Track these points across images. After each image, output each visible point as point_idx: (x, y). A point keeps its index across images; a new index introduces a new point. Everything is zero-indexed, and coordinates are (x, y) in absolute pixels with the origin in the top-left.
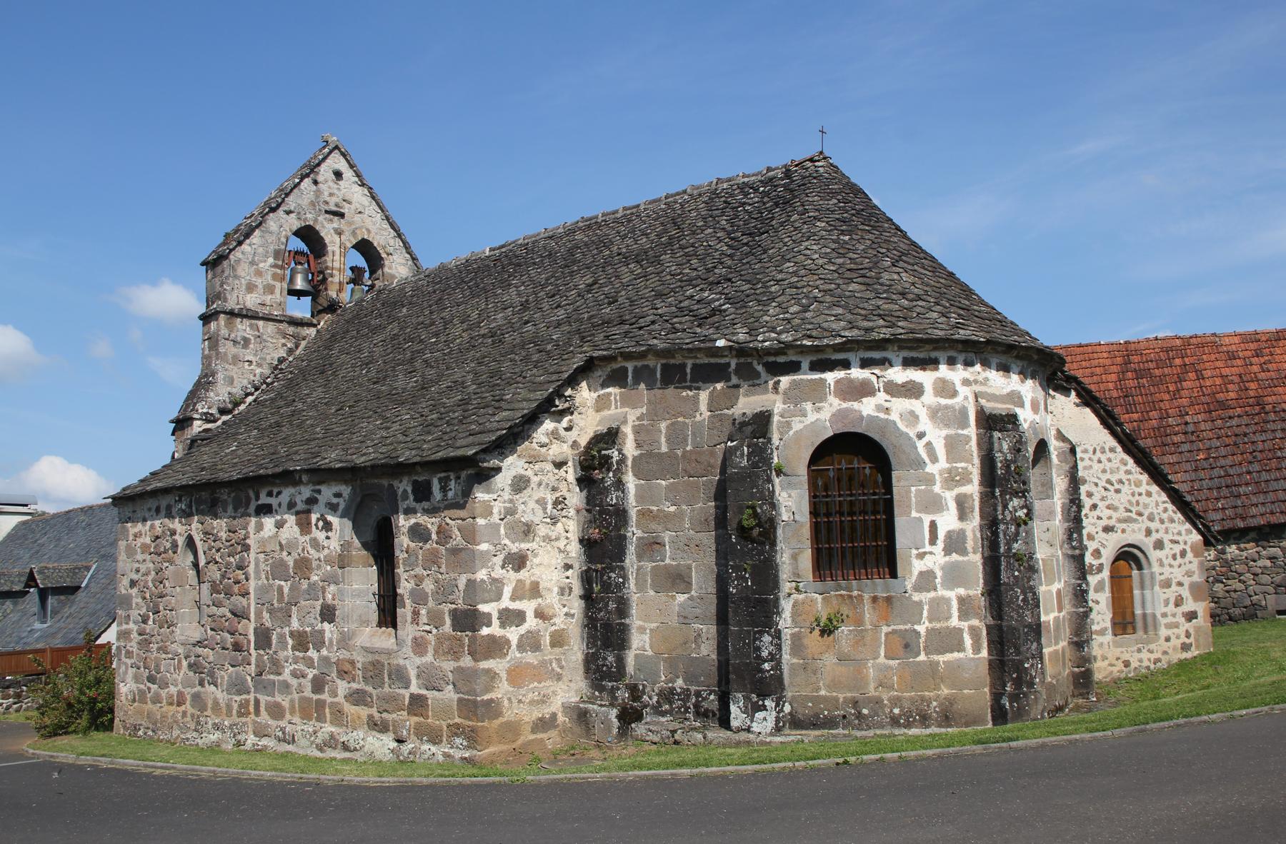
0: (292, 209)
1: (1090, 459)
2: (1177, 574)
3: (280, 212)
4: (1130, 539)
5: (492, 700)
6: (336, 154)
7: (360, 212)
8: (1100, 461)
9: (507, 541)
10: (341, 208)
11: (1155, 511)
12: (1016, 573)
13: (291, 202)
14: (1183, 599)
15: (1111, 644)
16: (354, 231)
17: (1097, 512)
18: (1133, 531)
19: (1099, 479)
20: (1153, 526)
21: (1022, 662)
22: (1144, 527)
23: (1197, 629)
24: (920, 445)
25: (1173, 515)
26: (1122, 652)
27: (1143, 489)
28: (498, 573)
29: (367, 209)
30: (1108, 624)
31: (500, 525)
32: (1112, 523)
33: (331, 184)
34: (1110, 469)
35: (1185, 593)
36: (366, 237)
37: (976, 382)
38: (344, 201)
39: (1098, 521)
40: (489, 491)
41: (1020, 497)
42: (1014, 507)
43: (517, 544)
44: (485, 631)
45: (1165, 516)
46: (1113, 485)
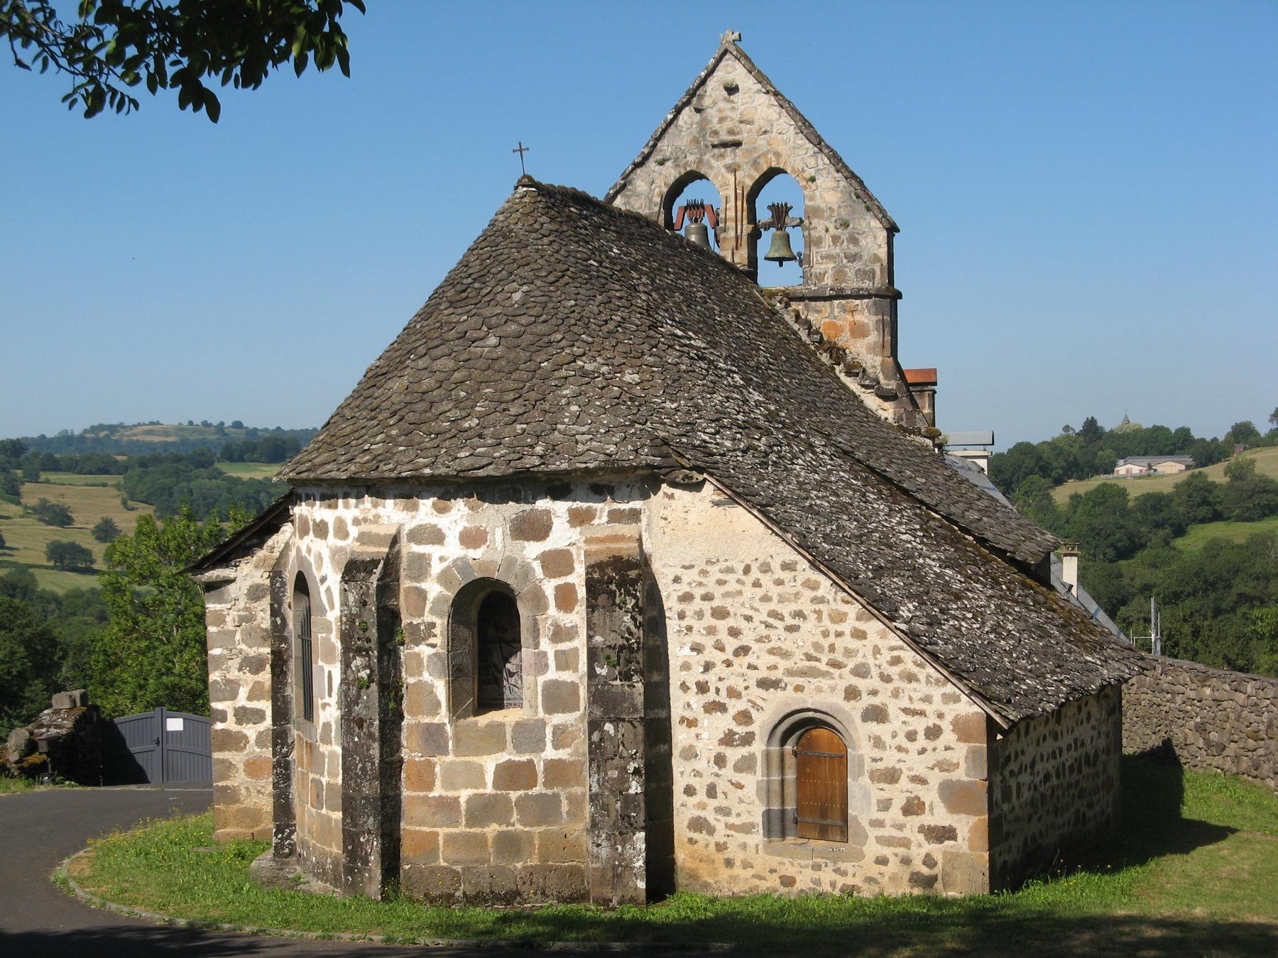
0: (668, 154)
1: (739, 581)
2: (915, 763)
3: (651, 164)
4: (810, 701)
5: (227, 787)
6: (728, 61)
7: (765, 132)
8: (757, 584)
9: (243, 646)
10: (738, 133)
11: (871, 661)
12: (356, 739)
13: (665, 147)
14: (923, 804)
15: (761, 847)
16: (755, 161)
17: (750, 659)
18: (819, 690)
19: (756, 610)
20: (862, 684)
21: (358, 835)
22: (842, 685)
23: (951, 858)
24: (323, 589)
25: (915, 670)
26: (781, 863)
27: (846, 627)
28: (234, 674)
29: (775, 124)
30: (758, 819)
31: (236, 631)
32: (773, 675)
33: (722, 105)
34: (779, 595)
35: (930, 795)
36: (773, 165)
37: (365, 520)
38: (741, 122)
39: (750, 672)
40: (220, 600)
41: (363, 656)
42: (357, 666)
43: (255, 649)
44: (219, 726)
45: (894, 671)
46: (782, 619)
